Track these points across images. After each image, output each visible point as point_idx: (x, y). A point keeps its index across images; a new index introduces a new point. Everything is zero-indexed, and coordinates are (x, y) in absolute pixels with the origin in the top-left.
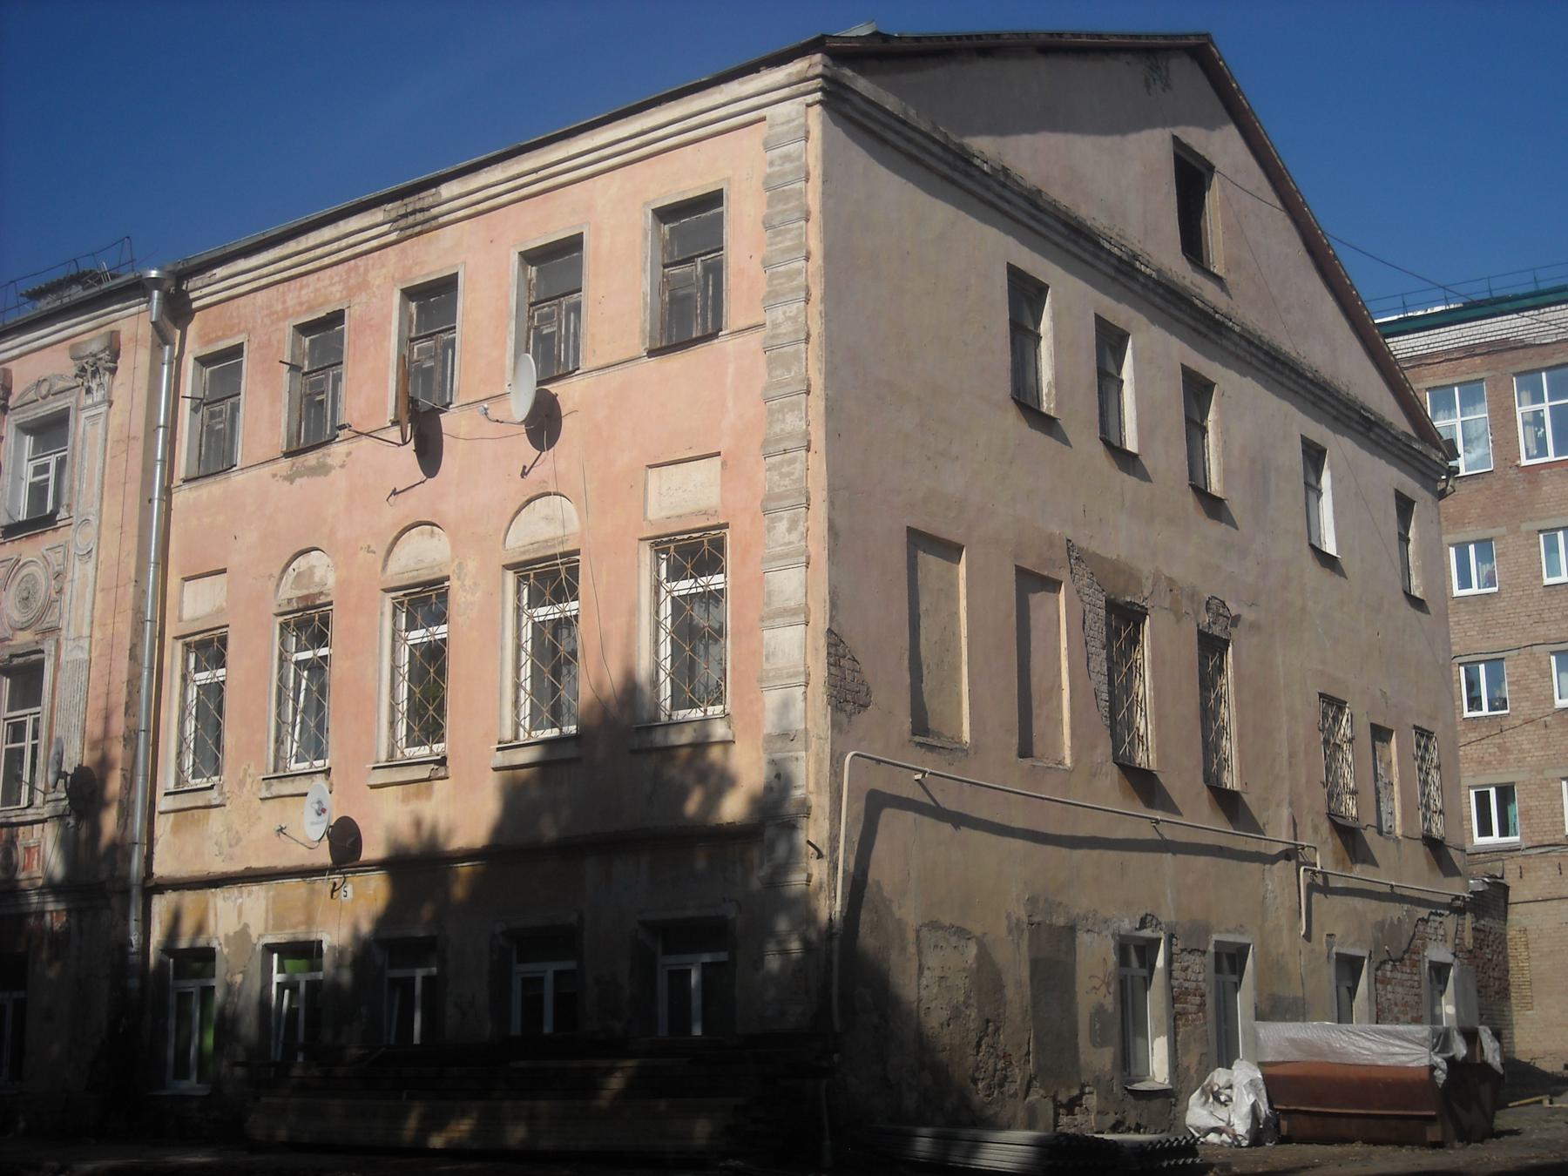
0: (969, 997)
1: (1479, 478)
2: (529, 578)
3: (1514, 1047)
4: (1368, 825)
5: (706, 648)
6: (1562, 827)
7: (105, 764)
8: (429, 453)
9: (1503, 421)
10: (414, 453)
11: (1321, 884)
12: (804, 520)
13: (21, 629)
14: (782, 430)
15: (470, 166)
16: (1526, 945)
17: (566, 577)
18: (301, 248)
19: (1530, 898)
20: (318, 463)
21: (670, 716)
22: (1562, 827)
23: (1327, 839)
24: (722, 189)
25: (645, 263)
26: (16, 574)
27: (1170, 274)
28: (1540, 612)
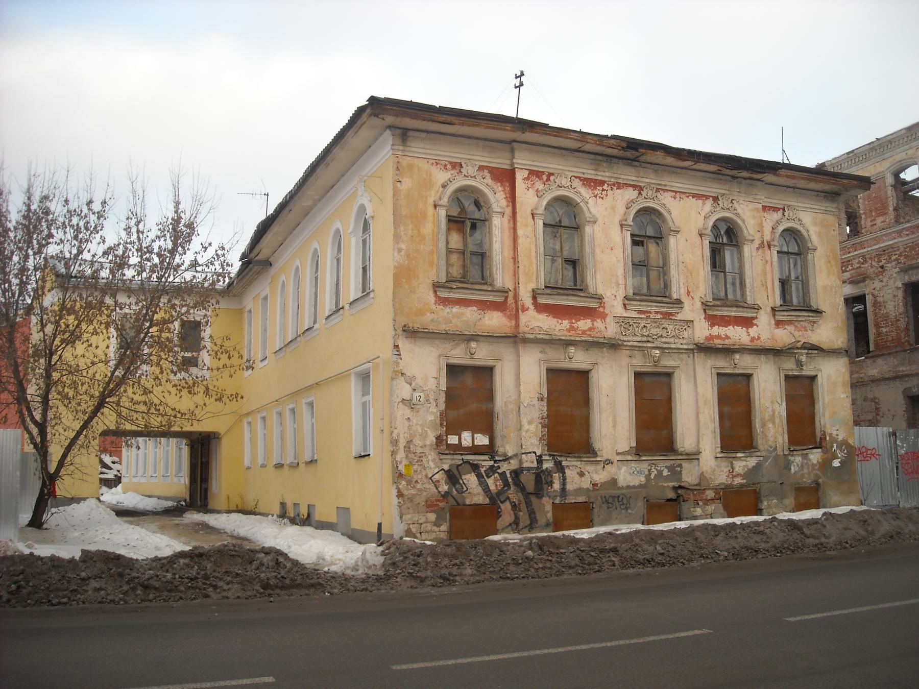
6: (732, 318)
11: (274, 680)
20: (191, 280)
23: (49, 291)
25: (505, 333)
26: (468, 137)
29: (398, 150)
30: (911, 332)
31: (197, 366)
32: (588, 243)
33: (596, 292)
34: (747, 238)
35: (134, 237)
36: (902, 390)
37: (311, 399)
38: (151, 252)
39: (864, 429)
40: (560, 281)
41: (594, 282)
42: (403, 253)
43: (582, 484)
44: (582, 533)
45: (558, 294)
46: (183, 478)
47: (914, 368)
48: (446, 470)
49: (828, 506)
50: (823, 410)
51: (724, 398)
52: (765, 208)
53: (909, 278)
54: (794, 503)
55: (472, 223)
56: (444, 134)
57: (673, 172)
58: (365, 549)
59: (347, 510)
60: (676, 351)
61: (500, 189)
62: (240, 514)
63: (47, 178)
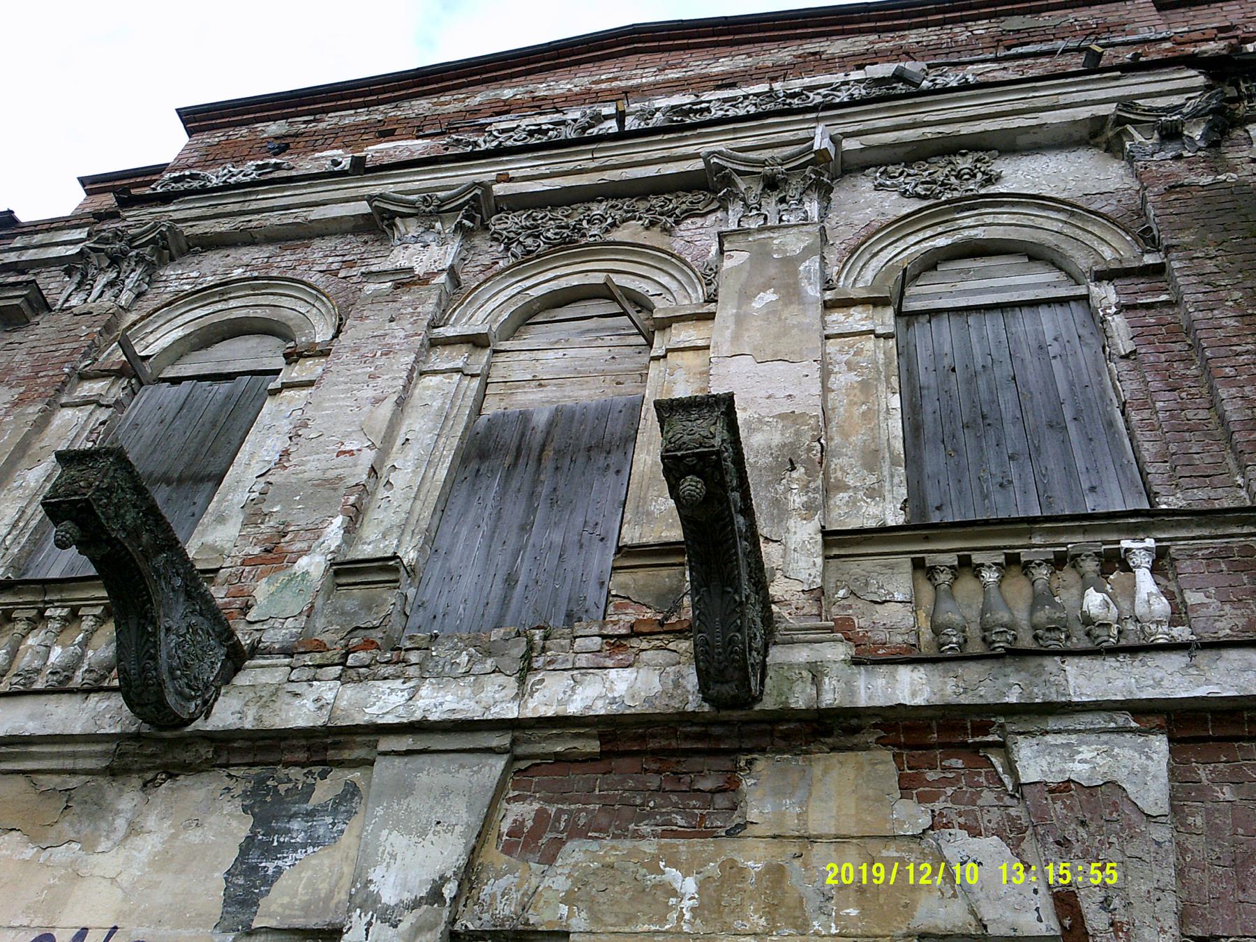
0: (1243, 614)
1: (1083, 249)
2: (972, 728)
3: (196, 518)
4: (668, 350)
5: (331, 893)
7: (1098, 554)
8: (791, 460)
9: (870, 876)
10: (5, 209)
12: (1057, 632)
13: (338, 332)
14: (531, 804)
15: (787, 29)
16: (942, 893)
17: (94, 243)
18: (188, 211)
19: (1044, 312)
21: (1139, 567)
22: (1088, 121)
24: (79, 178)
27: (226, 328)
28: (1064, 358)
29: (456, 535)
30: (542, 90)
31: (48, 308)
32: (1023, 37)
33: (775, 643)
34: (579, 689)
35: (314, 278)
36: (738, 287)
37: (622, 578)
38: (1130, 829)
39: (407, 265)
40: (927, 635)
41: (1035, 39)
42: (384, 481)
43: (262, 590)
44: (668, 168)
45: (310, 186)
46: (476, 383)
47: (1253, 530)
48: (242, 827)
49: (1088, 121)
50: (693, 724)
51: (310, 381)
52: (905, 270)
53: (259, 719)
54: (414, 719)
55: (913, 559)
56: (675, 277)
57: (866, 539)
58: (520, 696)
59: (714, 319)
60: (406, 743)
61: (105, 782)
62: (1031, 601)
63: (616, 340)
